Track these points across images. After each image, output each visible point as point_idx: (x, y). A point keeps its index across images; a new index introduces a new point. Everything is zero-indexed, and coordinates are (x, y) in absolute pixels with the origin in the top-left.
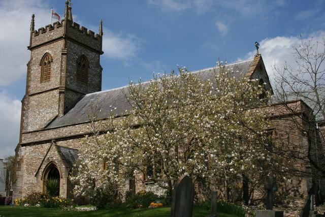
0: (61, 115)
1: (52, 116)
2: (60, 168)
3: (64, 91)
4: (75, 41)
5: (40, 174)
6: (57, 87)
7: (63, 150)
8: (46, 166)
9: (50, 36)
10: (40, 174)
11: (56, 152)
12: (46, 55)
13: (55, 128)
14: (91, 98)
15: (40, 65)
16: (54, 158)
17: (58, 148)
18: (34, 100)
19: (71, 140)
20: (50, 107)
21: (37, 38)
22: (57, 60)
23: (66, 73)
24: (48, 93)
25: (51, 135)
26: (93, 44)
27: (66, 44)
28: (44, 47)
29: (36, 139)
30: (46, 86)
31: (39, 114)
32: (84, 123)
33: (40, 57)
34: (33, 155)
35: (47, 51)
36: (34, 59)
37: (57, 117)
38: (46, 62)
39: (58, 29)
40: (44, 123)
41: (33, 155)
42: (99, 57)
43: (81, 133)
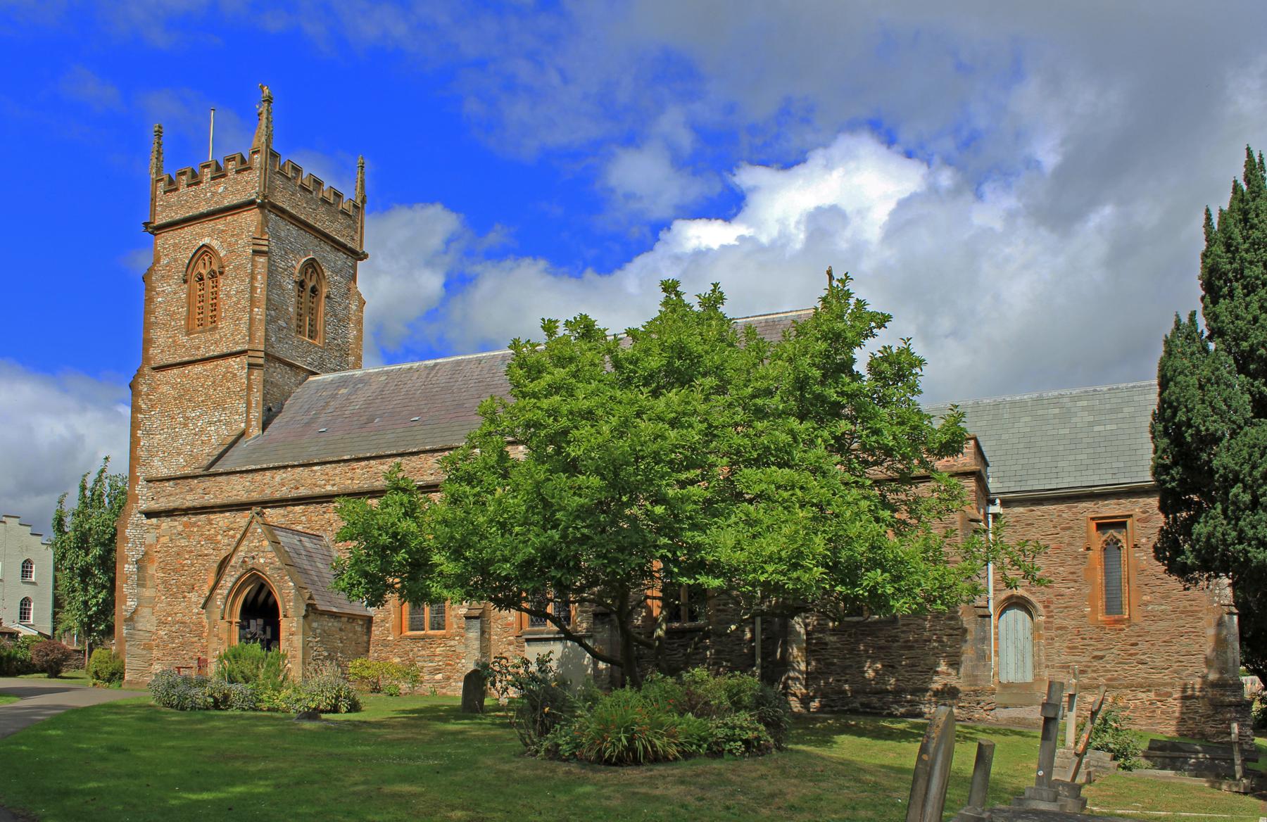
0: (255, 431)
1: (227, 433)
2: (281, 589)
3: (261, 361)
4: (292, 216)
5: (219, 602)
6: (239, 349)
7: (283, 537)
8: (235, 583)
9: (214, 194)
10: (219, 602)
11: (266, 543)
12: (205, 250)
13: (247, 472)
14: (338, 388)
15: (185, 282)
16: (262, 561)
17: (270, 528)
18: (168, 383)
19: (298, 509)
20: (220, 405)
21: (173, 197)
22: (236, 268)
23: (267, 309)
24: (210, 366)
25: (237, 489)
26: (1109, 609)
27: (265, 222)
28: (196, 228)
29: (190, 500)
30: (206, 345)
31: (186, 425)
32: (338, 462)
33: (185, 257)
34: (183, 543)
35: (206, 241)
36: (164, 261)
37: (243, 434)
38: (204, 272)
39: (239, 177)
40: (206, 452)
41: (183, 543)
42: (354, 267)
43: (329, 488)
